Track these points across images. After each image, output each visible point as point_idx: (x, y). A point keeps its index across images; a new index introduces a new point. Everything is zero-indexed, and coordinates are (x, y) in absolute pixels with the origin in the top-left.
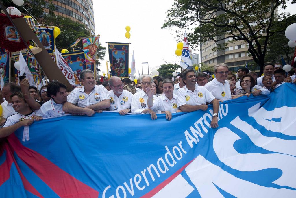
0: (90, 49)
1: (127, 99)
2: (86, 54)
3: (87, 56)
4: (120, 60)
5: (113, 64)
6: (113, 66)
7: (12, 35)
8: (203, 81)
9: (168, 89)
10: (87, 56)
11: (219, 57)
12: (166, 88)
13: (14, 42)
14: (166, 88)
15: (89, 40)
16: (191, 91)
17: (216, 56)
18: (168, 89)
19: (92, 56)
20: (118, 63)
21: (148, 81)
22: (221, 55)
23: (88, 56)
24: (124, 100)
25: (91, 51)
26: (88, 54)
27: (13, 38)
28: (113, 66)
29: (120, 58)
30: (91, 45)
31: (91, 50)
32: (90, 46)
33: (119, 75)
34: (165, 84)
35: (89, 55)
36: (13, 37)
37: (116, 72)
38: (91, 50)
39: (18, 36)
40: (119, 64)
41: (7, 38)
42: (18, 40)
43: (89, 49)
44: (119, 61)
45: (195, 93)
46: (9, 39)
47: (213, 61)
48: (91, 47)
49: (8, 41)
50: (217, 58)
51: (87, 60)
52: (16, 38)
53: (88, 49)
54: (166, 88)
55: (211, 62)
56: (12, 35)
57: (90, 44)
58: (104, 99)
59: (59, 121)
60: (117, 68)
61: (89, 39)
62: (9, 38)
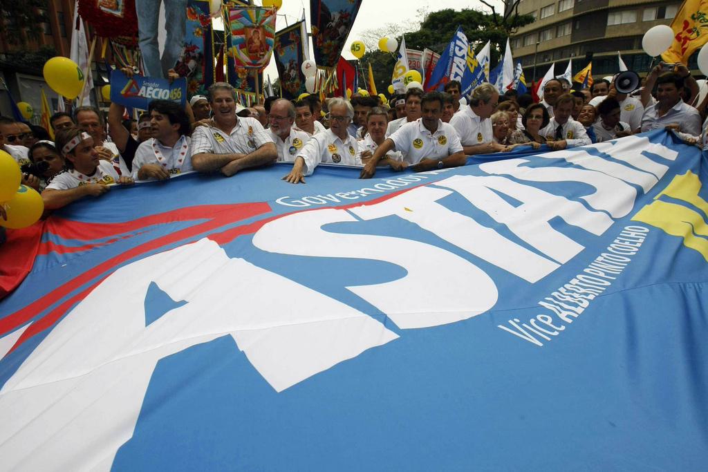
0: (249, 37)
1: (300, 142)
2: (238, 46)
3: (238, 52)
4: (341, 18)
5: (320, 28)
6: (320, 33)
7: (110, 3)
8: (447, 110)
9: (377, 126)
10: (238, 52)
11: (579, 16)
12: (373, 124)
13: (111, 16)
14: (373, 124)
15: (247, 12)
16: (430, 132)
17: (571, 15)
18: (377, 126)
19: (251, 54)
20: (333, 24)
21: (339, 114)
22: (582, 13)
23: (240, 51)
24: (295, 144)
25: (251, 41)
26: (241, 47)
27: (111, 8)
28: (320, 33)
29: (341, 12)
30: (253, 27)
31: (251, 38)
32: (248, 29)
33: (332, 61)
34: (373, 116)
35: (245, 49)
36: (111, 5)
37: (325, 53)
38: (251, 38)
39: (120, 7)
40: (335, 30)
41: (98, 4)
42: (118, 14)
43: (246, 36)
44: (337, 20)
45: (436, 136)
46: (103, 8)
47: (538, 35)
48: (252, 31)
49: (102, 12)
50: (574, 20)
51: (239, 63)
52: (117, 9)
53: (243, 36)
54: (375, 125)
55: (549, 36)
56: (110, 3)
57: (250, 24)
58: (263, 142)
59: (631, 169)
60: (328, 41)
61: (249, 11)
62: (102, 6)
